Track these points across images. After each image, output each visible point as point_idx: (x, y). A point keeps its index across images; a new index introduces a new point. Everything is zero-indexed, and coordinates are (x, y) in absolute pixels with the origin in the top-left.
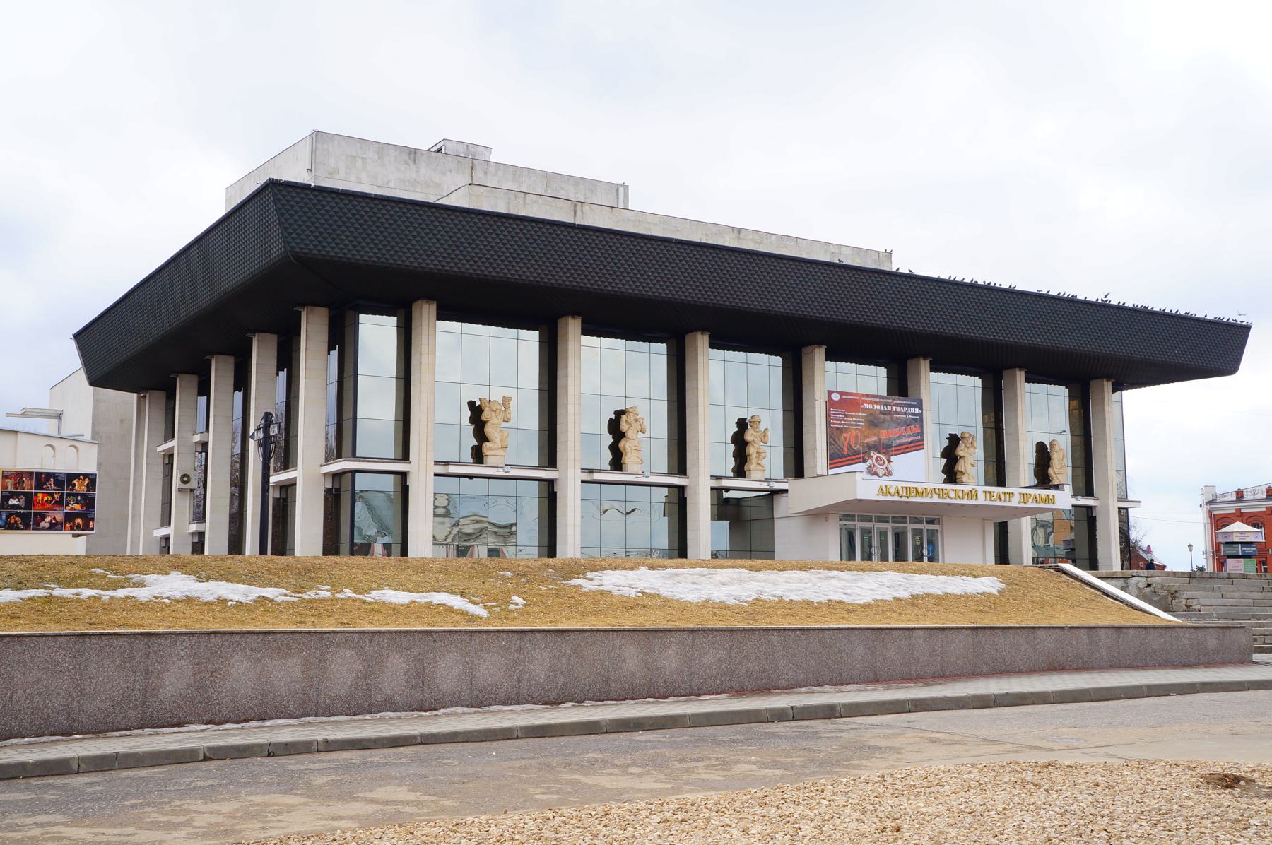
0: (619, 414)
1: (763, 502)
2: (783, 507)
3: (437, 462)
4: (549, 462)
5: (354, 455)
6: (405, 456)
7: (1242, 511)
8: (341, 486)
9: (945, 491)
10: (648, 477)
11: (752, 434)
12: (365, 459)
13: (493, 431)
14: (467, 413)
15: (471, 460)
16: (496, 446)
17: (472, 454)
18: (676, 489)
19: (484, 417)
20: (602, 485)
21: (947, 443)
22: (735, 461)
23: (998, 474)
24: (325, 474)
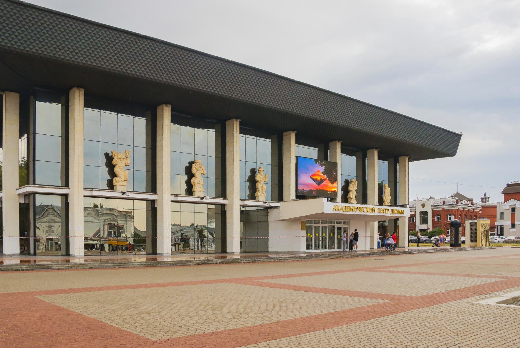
0: (191, 163)
1: (262, 213)
2: (273, 215)
3: (85, 189)
4: (152, 190)
5: (34, 183)
6: (66, 184)
7: (445, 209)
8: (29, 202)
9: (348, 207)
10: (208, 199)
11: (260, 177)
12: (40, 186)
13: (119, 170)
14: (104, 160)
15: (107, 188)
16: (121, 180)
17: (107, 184)
18: (150, 202)
19: (114, 162)
20: (208, 205)
21: (344, 184)
22: (250, 191)
23: (363, 199)
24: (19, 195)
